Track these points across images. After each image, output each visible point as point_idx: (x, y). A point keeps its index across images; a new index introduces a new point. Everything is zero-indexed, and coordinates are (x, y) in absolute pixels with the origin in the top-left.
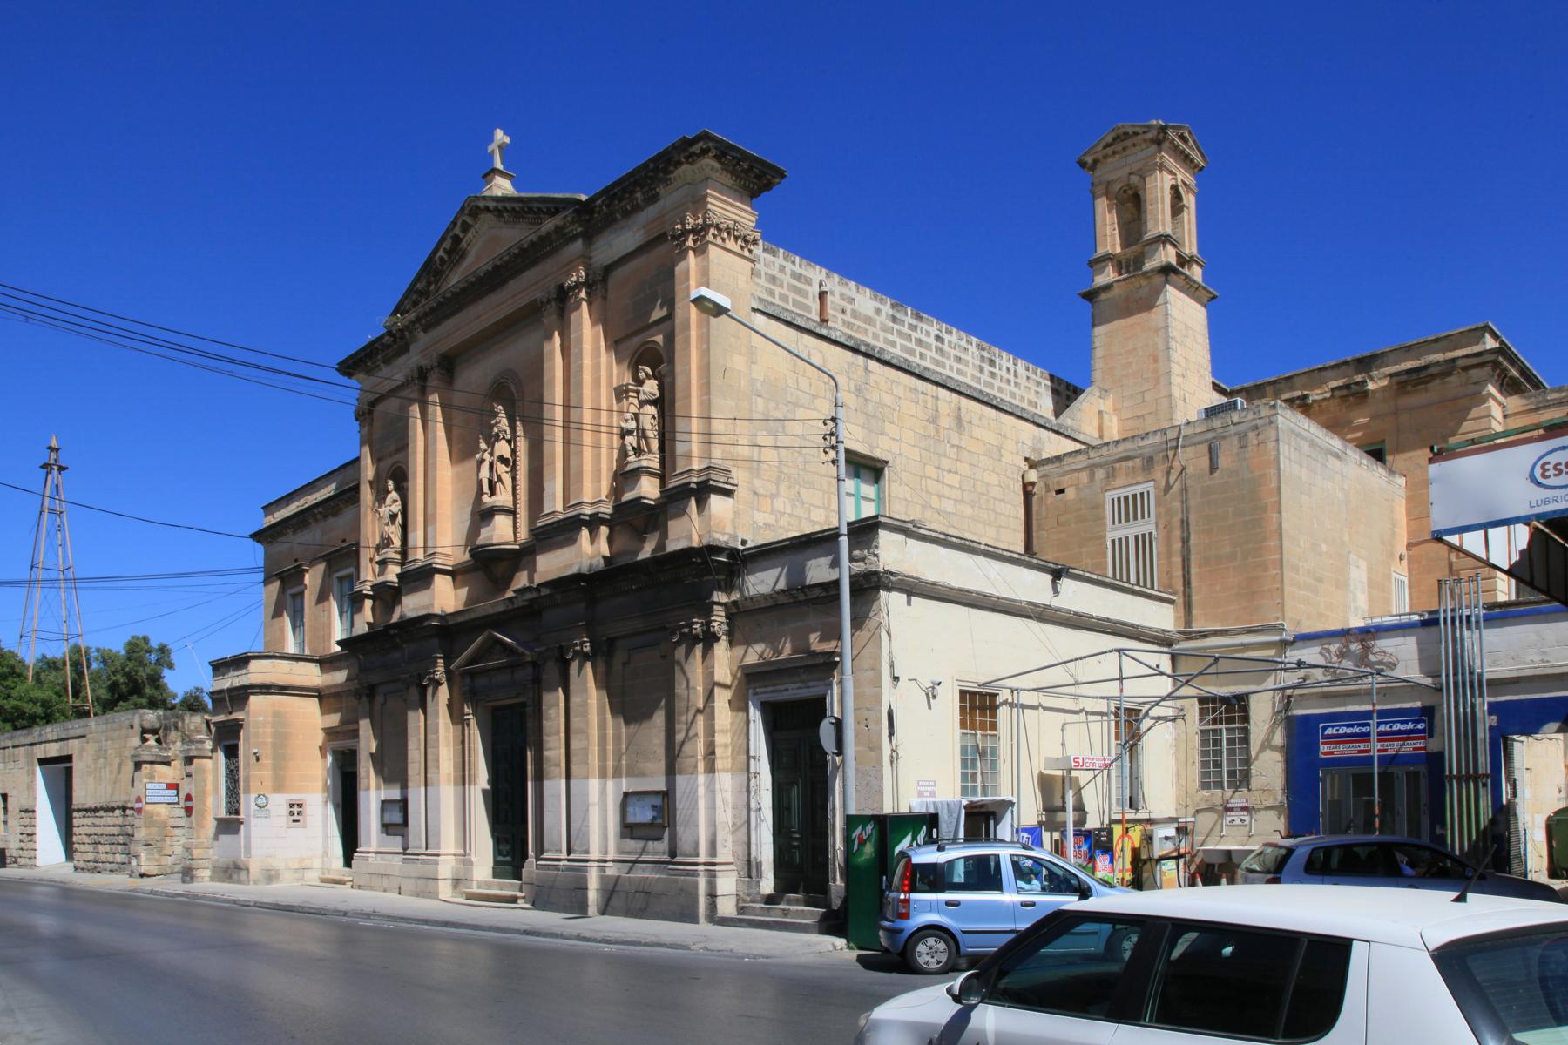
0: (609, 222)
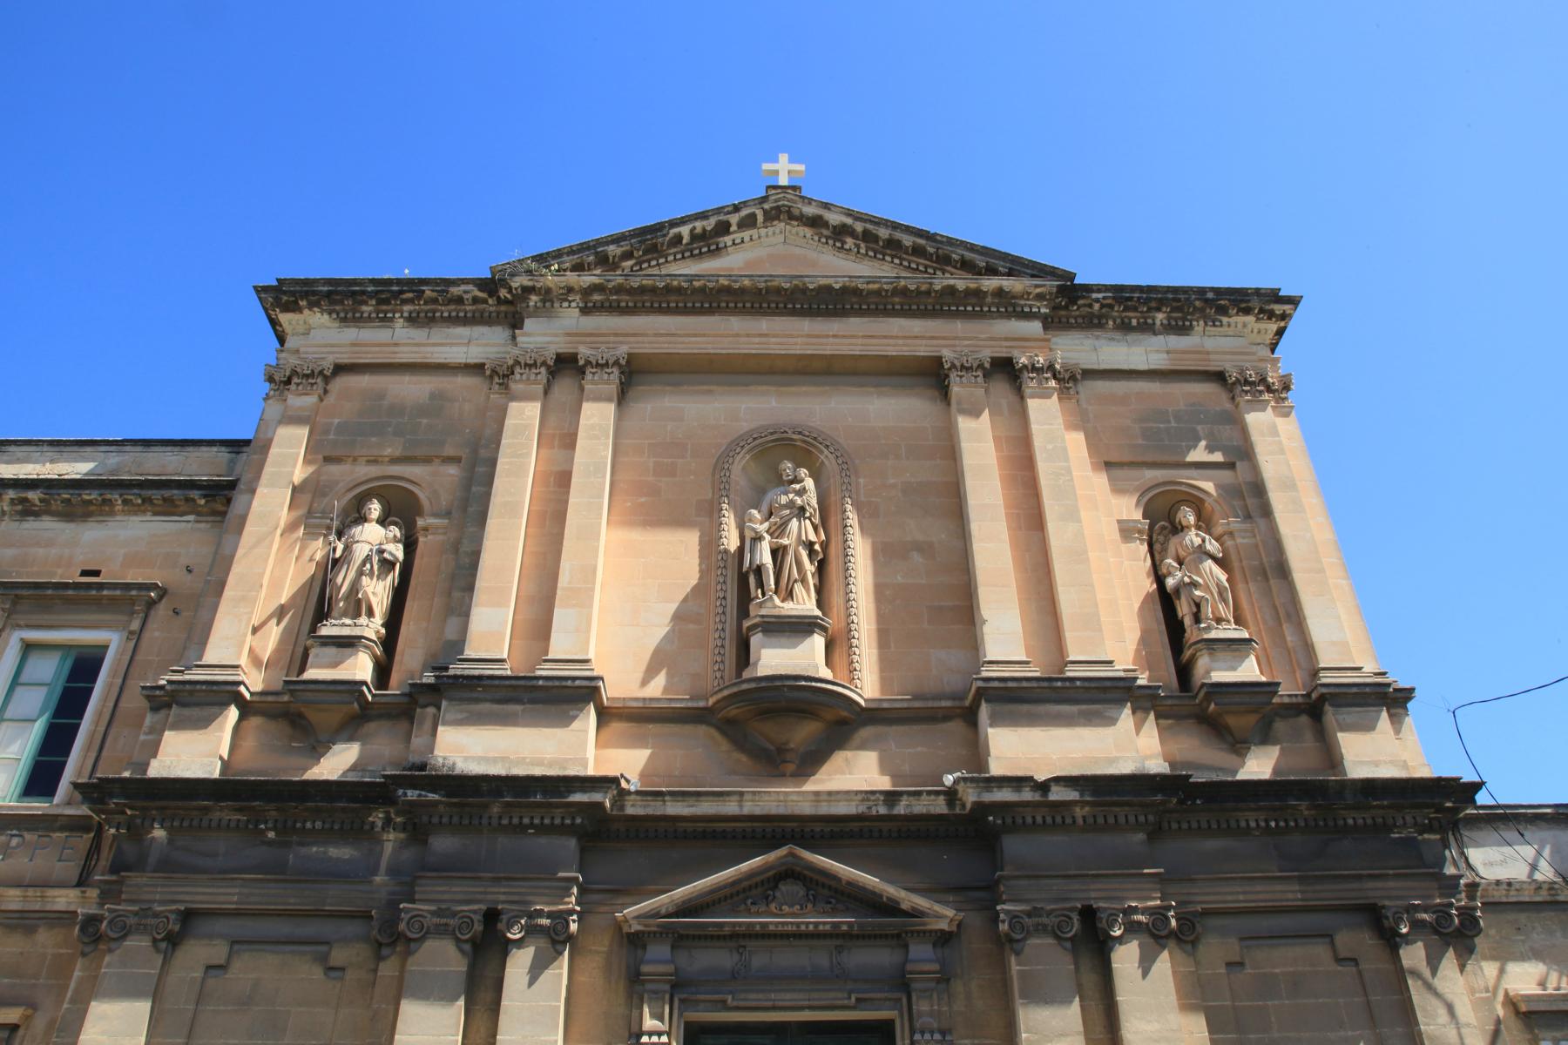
0: (1092, 323)
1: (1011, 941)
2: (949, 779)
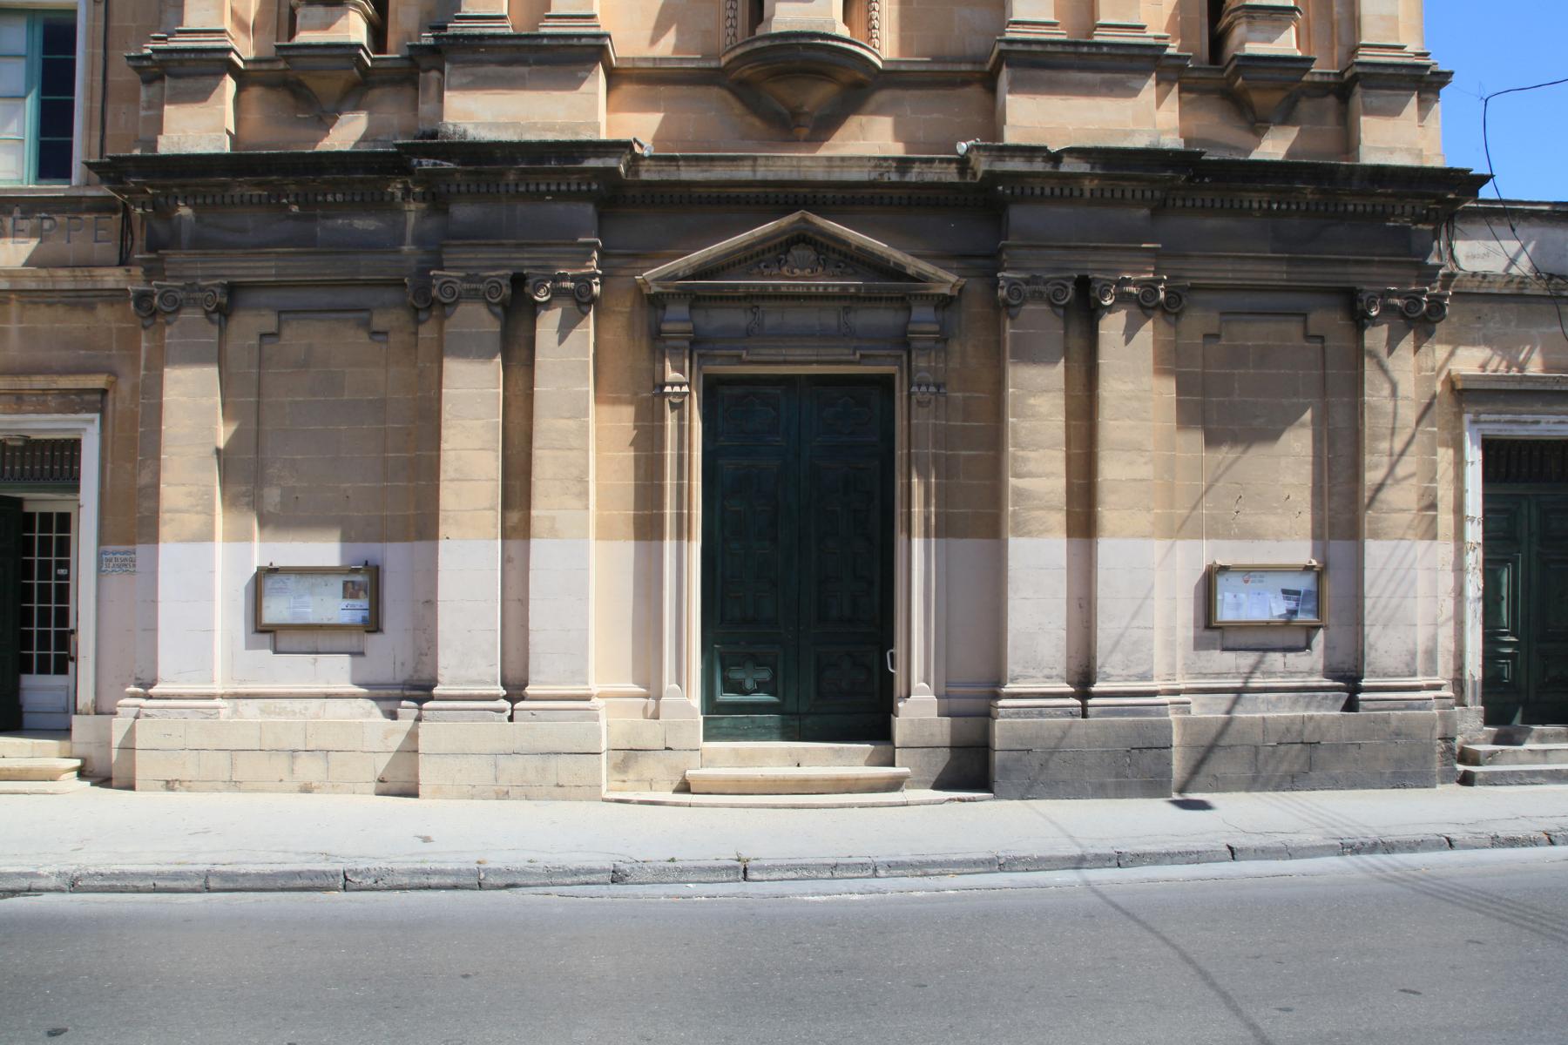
1: (1008, 306)
2: (962, 147)
